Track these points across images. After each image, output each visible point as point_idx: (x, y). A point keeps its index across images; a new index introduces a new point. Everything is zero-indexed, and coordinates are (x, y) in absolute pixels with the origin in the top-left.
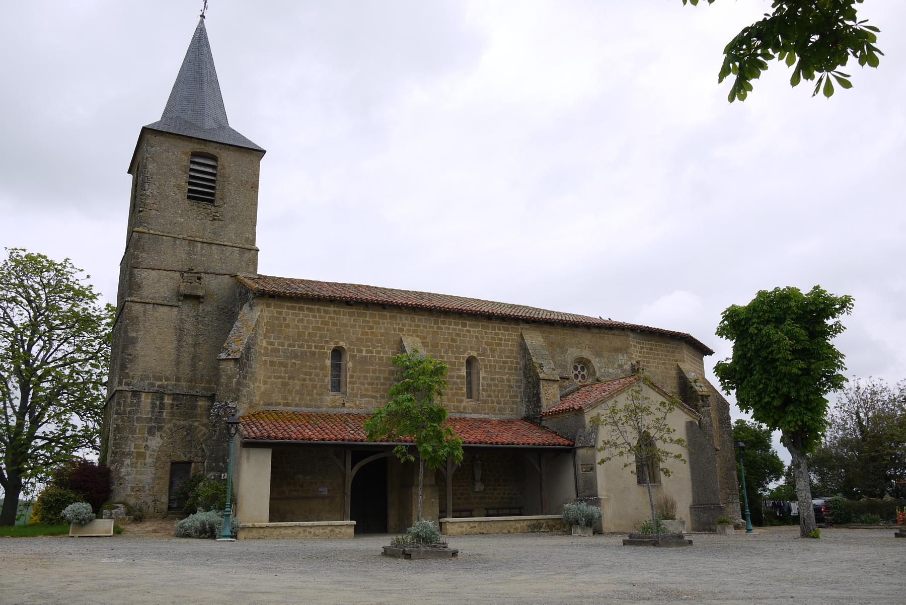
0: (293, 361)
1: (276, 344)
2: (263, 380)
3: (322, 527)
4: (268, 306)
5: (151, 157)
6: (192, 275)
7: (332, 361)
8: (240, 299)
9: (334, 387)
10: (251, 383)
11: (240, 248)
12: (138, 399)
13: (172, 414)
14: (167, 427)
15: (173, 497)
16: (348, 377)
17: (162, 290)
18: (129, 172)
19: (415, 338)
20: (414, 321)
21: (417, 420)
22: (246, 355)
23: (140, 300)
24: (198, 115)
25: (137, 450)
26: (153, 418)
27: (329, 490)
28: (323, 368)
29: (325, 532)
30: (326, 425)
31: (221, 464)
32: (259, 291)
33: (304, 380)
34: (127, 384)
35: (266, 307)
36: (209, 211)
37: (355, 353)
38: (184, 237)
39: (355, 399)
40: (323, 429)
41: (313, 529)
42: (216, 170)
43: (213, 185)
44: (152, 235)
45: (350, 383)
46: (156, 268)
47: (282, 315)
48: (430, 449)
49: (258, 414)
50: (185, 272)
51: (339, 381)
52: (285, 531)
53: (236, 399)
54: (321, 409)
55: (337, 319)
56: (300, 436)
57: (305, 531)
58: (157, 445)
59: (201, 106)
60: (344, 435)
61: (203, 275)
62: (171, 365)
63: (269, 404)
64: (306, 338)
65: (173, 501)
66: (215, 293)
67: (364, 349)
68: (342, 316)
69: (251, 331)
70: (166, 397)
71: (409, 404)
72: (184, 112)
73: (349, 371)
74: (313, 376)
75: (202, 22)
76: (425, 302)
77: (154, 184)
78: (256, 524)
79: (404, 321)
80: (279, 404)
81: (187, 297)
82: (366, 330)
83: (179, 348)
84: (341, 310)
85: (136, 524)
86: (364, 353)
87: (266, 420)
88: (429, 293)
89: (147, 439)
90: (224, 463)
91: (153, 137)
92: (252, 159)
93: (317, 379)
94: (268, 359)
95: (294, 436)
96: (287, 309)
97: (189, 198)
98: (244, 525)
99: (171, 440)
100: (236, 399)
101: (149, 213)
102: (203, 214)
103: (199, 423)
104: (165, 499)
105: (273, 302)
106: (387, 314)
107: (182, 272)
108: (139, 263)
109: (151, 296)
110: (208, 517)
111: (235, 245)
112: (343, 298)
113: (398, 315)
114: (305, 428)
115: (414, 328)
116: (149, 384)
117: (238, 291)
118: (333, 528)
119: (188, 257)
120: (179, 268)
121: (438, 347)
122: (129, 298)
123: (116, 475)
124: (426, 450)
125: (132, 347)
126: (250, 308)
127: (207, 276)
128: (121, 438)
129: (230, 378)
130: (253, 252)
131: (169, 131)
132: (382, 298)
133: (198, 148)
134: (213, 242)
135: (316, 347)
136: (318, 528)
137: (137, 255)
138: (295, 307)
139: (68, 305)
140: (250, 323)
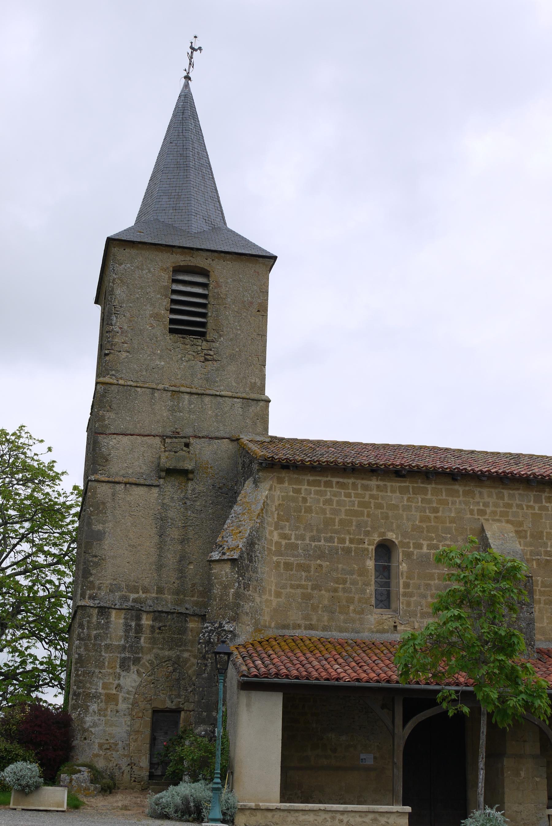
0: (319, 562)
1: (293, 537)
2: (275, 591)
3: (359, 814)
4: (280, 481)
5: (120, 279)
6: (176, 440)
7: (376, 560)
9: (381, 601)
10: (256, 595)
11: (243, 398)
12: (107, 619)
13: (153, 641)
14: (146, 658)
15: (155, 760)
16: (401, 586)
17: (137, 463)
18: (97, 302)
19: (504, 524)
20: (502, 498)
22: (248, 554)
23: (107, 479)
24: (182, 214)
25: (106, 691)
26: (127, 645)
27: (375, 758)
28: (363, 572)
29: (364, 822)
30: (366, 658)
32: (266, 460)
33: (335, 590)
34: (92, 598)
35: (277, 484)
36: (199, 348)
37: (411, 550)
38: (164, 388)
39: (412, 619)
40: (360, 665)
41: (346, 816)
42: (208, 289)
45: (405, 595)
46: (128, 432)
47: (301, 494)
48: (494, 695)
49: (267, 641)
50: (167, 437)
51: (389, 593)
52: (304, 817)
53: (235, 619)
54: (361, 635)
56: (324, 674)
57: (333, 818)
58: (133, 685)
59: (187, 202)
60: (390, 673)
61: (192, 440)
63: (286, 627)
64: (336, 527)
65: (156, 766)
66: (209, 466)
67: (425, 543)
68: (389, 494)
70: (144, 616)
71: (458, 624)
72: (164, 212)
73: (403, 578)
74: (348, 585)
75: (186, 86)
76: (521, 470)
77: (125, 316)
78: (261, 804)
79: (487, 499)
80: (299, 626)
81: (171, 472)
82: (428, 514)
83: (161, 547)
84: (389, 484)
85: (103, 796)
86: (425, 550)
87: (278, 649)
88: (530, 455)
89: (120, 675)
91: (122, 250)
93: (353, 590)
94: (282, 559)
95: (315, 674)
96: (308, 485)
98: (245, 805)
99: (152, 677)
100: (235, 619)
102: (191, 353)
103: (189, 653)
104: (144, 762)
105: (287, 475)
106: (459, 488)
107: (163, 437)
108: (106, 426)
109: (122, 472)
110: (193, 791)
111: (236, 395)
112: (389, 466)
113: (477, 490)
114: (333, 662)
115: (502, 510)
116: (121, 598)
117: (240, 461)
118: (377, 816)
119: (172, 415)
120: (160, 430)
121: (541, 537)
122: (93, 477)
123: (78, 725)
124: (488, 696)
125: (98, 545)
126: (254, 485)
127: (198, 440)
128: (84, 673)
129: (226, 588)
130: (262, 404)
131: (143, 240)
132: (453, 464)
133: (182, 260)
134: (204, 392)
135: (351, 541)
136: (353, 814)
137: (102, 416)
138: (320, 481)
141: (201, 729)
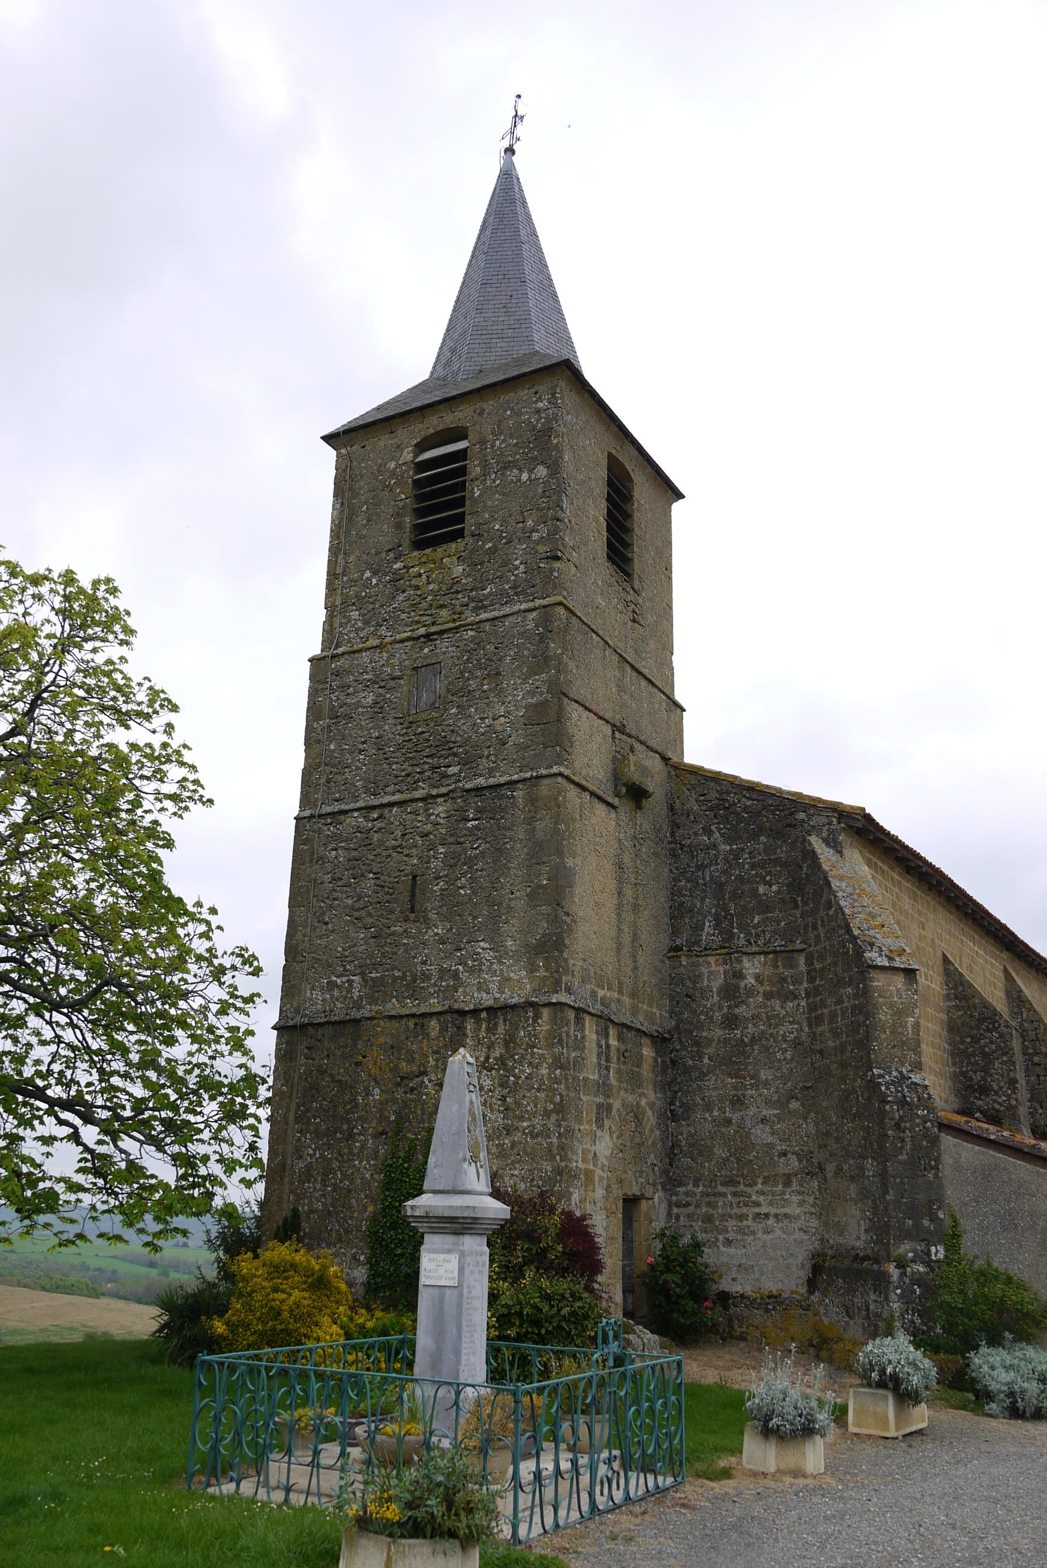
21: (227, 962)
31: (926, 1223)
90: (931, 1220)
141: (668, 1233)
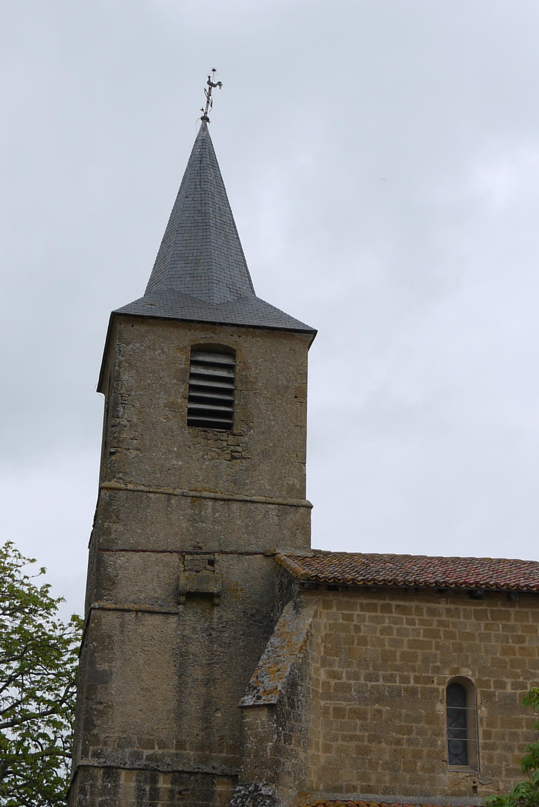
0: (377, 706)
1: (344, 675)
4: (327, 605)
5: (127, 361)
6: (198, 557)
7: (448, 704)
8: (282, 595)
10: (300, 749)
11: (279, 504)
12: (115, 781)
18: (99, 390)
22: (289, 698)
23: (113, 606)
24: (202, 282)
28: (432, 719)
32: (309, 579)
33: (398, 742)
34: (97, 755)
36: (225, 444)
37: (492, 689)
39: (495, 778)
42: (233, 372)
43: (229, 398)
44: (131, 493)
45: (486, 747)
46: (140, 548)
50: (188, 553)
51: (465, 745)
53: (274, 780)
55: (454, 625)
59: (206, 267)
61: (217, 557)
62: (167, 719)
63: (337, 789)
67: (509, 681)
68: (462, 620)
69: (296, 653)
70: (161, 778)
72: (179, 279)
74: (414, 735)
75: (204, 128)
77: (134, 406)
80: (354, 788)
82: (511, 644)
84: (461, 607)
86: (509, 690)
91: (129, 327)
92: (293, 348)
93: (421, 741)
96: (361, 610)
97: (191, 423)
100: (274, 780)
101: (126, 454)
102: (214, 449)
105: (335, 597)
107: (182, 554)
109: (133, 597)
111: (270, 500)
112: (461, 584)
117: (277, 581)
119: (192, 526)
122: (96, 604)
125: (104, 689)
126: (295, 611)
127: (224, 557)
129: (262, 741)
130: (302, 510)
134: (232, 498)
135: (417, 680)
137: (107, 529)
138: (375, 605)
139: (16, 622)
140: (294, 637)
